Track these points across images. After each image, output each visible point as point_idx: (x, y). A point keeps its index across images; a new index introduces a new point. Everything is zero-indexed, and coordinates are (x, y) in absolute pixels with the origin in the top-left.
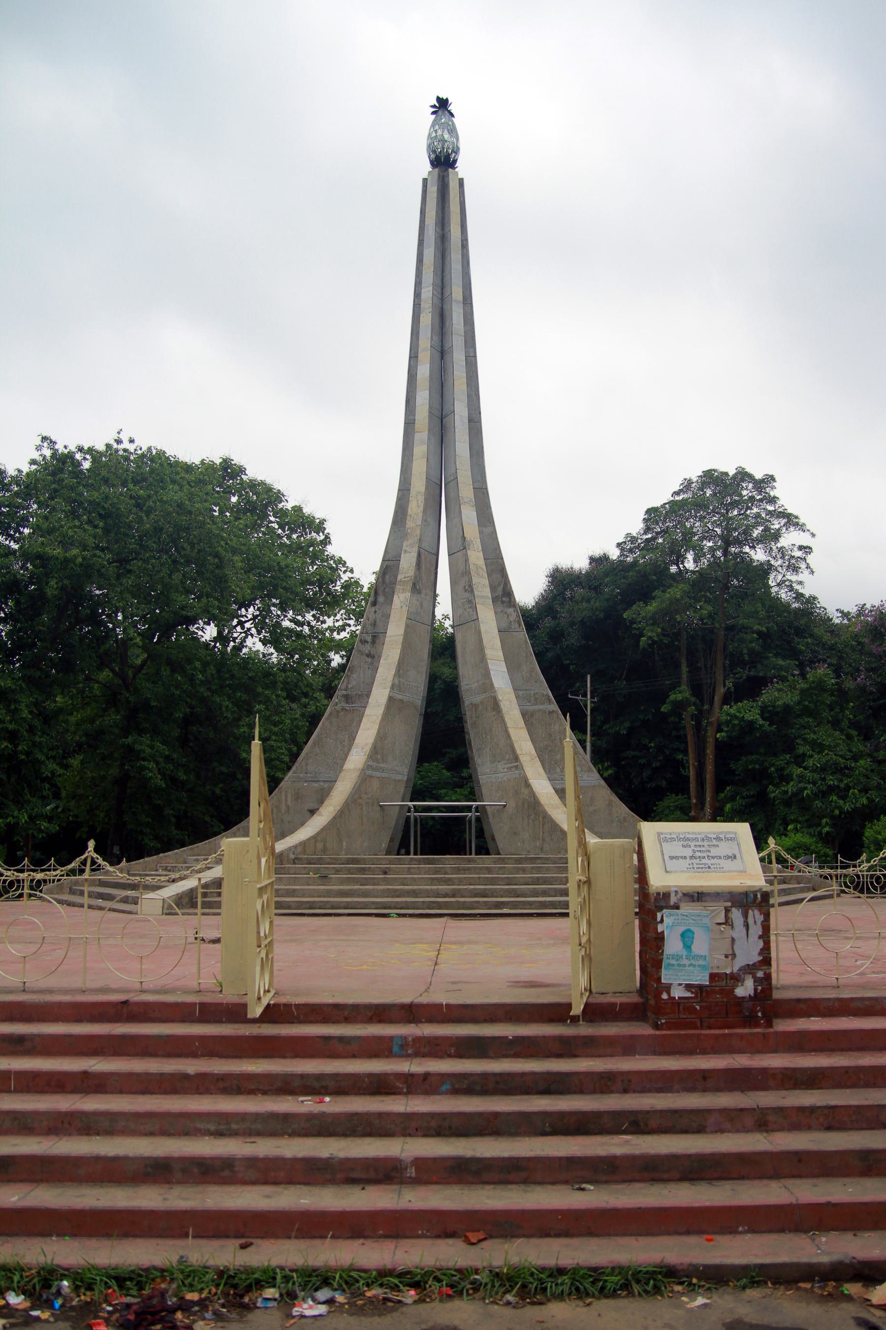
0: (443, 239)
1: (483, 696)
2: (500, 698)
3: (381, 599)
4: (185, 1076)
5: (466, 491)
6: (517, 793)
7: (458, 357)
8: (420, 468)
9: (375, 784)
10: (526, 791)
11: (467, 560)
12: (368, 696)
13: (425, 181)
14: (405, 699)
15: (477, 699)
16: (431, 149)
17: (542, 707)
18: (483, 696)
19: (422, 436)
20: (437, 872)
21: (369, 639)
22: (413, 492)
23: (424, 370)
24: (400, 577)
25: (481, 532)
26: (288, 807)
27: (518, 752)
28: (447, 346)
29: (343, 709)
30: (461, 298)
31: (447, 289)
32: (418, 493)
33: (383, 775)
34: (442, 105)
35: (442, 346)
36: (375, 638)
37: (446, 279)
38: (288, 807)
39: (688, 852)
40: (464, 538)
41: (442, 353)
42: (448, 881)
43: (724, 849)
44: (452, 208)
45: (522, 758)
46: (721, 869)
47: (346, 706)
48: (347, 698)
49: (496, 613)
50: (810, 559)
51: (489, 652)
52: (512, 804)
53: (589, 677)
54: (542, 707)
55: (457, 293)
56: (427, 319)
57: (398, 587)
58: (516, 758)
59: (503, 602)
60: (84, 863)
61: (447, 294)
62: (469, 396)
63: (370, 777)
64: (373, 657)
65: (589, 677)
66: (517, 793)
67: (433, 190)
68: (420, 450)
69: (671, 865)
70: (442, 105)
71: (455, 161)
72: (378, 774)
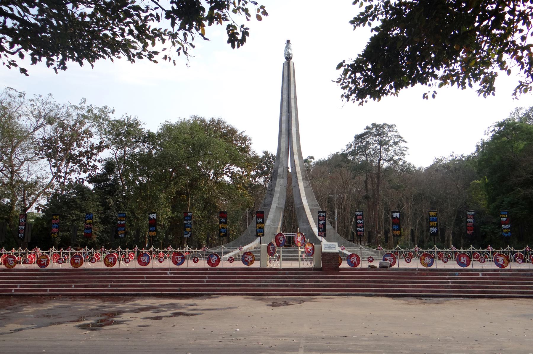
0: (289, 80)
1: (300, 206)
2: (304, 206)
3: (273, 179)
4: (259, 276)
5: (295, 151)
6: (309, 231)
7: (293, 114)
8: (283, 145)
9: (273, 229)
10: (311, 231)
11: (296, 170)
12: (271, 204)
13: (284, 64)
14: (280, 206)
15: (299, 206)
16: (285, 54)
17: (316, 208)
18: (300, 206)
19: (284, 136)
20: (289, 251)
21: (270, 190)
22: (281, 151)
23: (284, 118)
24: (278, 174)
25: (299, 161)
26: (249, 234)
27: (309, 221)
28: (290, 100)
29: (264, 208)
30: (294, 97)
31: (290, 95)
32: (283, 151)
33: (275, 226)
34: (288, 42)
35: (289, 100)
36: (272, 189)
37: (290, 92)
38: (249, 234)
39: (328, 247)
40: (295, 164)
41: (289, 112)
42: (291, 253)
43: (333, 246)
44: (291, 72)
45: (310, 222)
46: (332, 249)
47: (264, 208)
48: (264, 205)
49: (303, 183)
50: (408, 150)
51: (302, 194)
52: (308, 234)
53: (463, 49)
54: (316, 208)
55: (293, 96)
56: (285, 104)
57: (278, 177)
58: (309, 222)
59: (305, 180)
60: (515, 252)
61: (290, 96)
62: (296, 124)
63: (272, 227)
64: (271, 195)
65: (463, 49)
66: (309, 231)
67: (286, 67)
68: (283, 140)
69: (325, 248)
70: (288, 42)
71: (292, 58)
72: (274, 226)
